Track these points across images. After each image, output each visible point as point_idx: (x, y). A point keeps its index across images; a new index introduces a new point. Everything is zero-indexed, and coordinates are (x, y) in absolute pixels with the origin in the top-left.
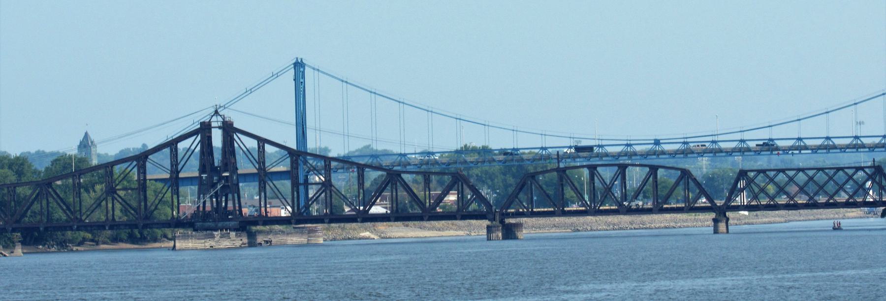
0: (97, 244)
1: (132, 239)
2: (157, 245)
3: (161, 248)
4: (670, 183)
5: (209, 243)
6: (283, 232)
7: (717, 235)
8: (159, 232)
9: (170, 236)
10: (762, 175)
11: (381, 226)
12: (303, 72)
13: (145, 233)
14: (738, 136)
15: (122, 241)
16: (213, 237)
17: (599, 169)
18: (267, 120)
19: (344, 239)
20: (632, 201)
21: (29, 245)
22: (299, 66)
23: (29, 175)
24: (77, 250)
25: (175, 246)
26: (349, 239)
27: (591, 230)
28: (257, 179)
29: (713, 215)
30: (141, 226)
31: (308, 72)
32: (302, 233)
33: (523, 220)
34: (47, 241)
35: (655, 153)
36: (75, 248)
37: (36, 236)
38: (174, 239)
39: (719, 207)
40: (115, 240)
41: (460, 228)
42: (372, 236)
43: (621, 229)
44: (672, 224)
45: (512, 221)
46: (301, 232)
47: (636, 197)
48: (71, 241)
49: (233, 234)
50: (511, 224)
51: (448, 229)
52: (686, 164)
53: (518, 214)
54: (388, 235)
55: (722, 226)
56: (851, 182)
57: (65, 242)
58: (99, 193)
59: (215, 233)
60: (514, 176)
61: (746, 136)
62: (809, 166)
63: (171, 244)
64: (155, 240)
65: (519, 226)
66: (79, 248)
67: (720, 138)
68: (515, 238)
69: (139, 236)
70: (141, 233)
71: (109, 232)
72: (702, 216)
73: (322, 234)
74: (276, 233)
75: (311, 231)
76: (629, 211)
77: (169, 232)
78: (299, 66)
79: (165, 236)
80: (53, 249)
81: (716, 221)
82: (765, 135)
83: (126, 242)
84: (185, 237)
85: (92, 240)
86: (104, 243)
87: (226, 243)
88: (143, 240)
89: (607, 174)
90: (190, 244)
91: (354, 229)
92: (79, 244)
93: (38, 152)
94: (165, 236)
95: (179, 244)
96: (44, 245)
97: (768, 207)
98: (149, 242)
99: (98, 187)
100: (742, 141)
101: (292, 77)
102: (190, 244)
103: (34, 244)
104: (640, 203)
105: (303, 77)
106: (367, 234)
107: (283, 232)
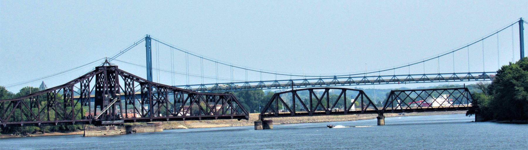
0: (43, 133)
1: (61, 130)
2: (74, 133)
3: (77, 135)
4: (320, 102)
5: (103, 133)
6: (142, 126)
7: (379, 127)
8: (75, 126)
9: (81, 128)
10: (413, 92)
11: (189, 122)
12: (150, 42)
13: (68, 127)
14: (377, 74)
15: (55, 131)
16: (105, 129)
17: (314, 90)
18: (133, 64)
19: (170, 129)
20: (333, 108)
21: (6, 134)
22: (148, 39)
23: (5, 96)
24: (32, 136)
25: (84, 134)
26: (173, 129)
27: (290, 123)
28: (124, 98)
29: (377, 115)
30: (66, 125)
31: (153, 42)
32: (152, 126)
33: (273, 119)
34: (15, 131)
35: (334, 83)
36: (30, 135)
37: (11, 130)
38: (84, 130)
39: (380, 111)
40: (52, 130)
41: (227, 123)
42: (184, 127)
43: (304, 123)
44: (327, 120)
45: (266, 119)
46: (151, 125)
47: (334, 106)
48: (29, 132)
49: (116, 127)
50: (266, 121)
51: (221, 123)
52: (363, 87)
53: (270, 116)
54: (192, 127)
55: (382, 121)
56: (408, 98)
57: (25, 132)
58: (44, 106)
59: (107, 127)
60: (244, 98)
61: (381, 74)
62: (367, 94)
63: (83, 132)
64: (74, 130)
65: (270, 122)
66: (33, 135)
67: (368, 75)
68: (268, 128)
69: (65, 128)
70: (66, 127)
71: (49, 127)
72: (370, 116)
73: (162, 127)
74: (138, 126)
75: (156, 125)
76: (331, 113)
77: (80, 126)
78: (148, 39)
79: (79, 128)
80: (19, 136)
81: (379, 118)
82: (392, 73)
83: (58, 131)
84: (90, 129)
85: (40, 131)
86: (46, 132)
87: (112, 133)
88: (67, 130)
89: (319, 92)
90: (93, 133)
91: (175, 124)
92: (34, 133)
93: (27, 93)
94: (79, 128)
95: (87, 133)
96: (14, 134)
97: (407, 111)
98: (70, 131)
99: (43, 103)
100: (380, 77)
101: (145, 45)
102: (93, 132)
103: (8, 133)
104: (337, 109)
105: (150, 45)
106: (182, 126)
107: (142, 126)
